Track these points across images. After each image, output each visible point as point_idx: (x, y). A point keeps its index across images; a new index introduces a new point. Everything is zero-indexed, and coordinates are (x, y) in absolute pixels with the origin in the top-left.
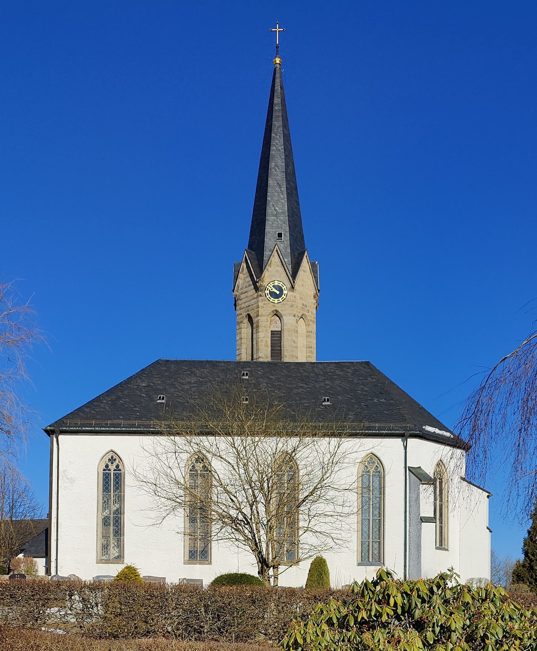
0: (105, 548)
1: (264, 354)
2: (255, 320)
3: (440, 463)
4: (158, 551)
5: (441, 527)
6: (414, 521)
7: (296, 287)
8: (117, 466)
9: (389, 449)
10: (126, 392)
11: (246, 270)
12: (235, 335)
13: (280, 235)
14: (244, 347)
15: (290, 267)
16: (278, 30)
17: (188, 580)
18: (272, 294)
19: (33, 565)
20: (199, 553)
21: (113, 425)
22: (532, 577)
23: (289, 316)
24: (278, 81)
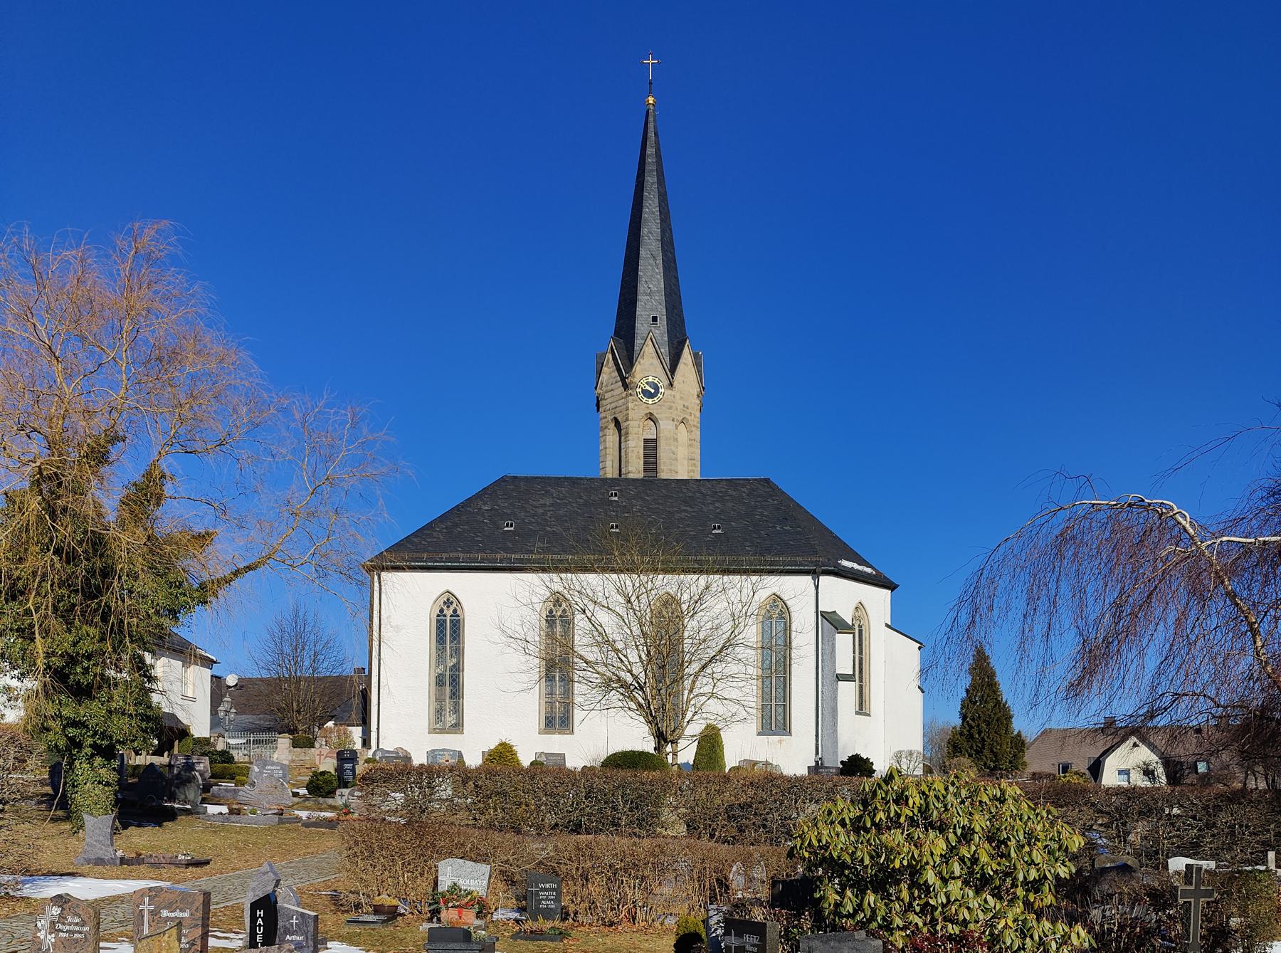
0: (439, 713)
1: (635, 469)
2: (623, 425)
3: (860, 607)
4: (504, 715)
5: (861, 687)
6: (828, 679)
7: (675, 384)
8: (455, 611)
9: (795, 588)
10: (464, 518)
11: (611, 363)
12: (598, 444)
13: (655, 319)
14: (609, 458)
15: (667, 359)
16: (651, 62)
17: (547, 755)
18: (645, 392)
19: (347, 735)
20: (558, 719)
21: (449, 560)
22: (971, 748)
23: (667, 421)
24: (651, 125)
